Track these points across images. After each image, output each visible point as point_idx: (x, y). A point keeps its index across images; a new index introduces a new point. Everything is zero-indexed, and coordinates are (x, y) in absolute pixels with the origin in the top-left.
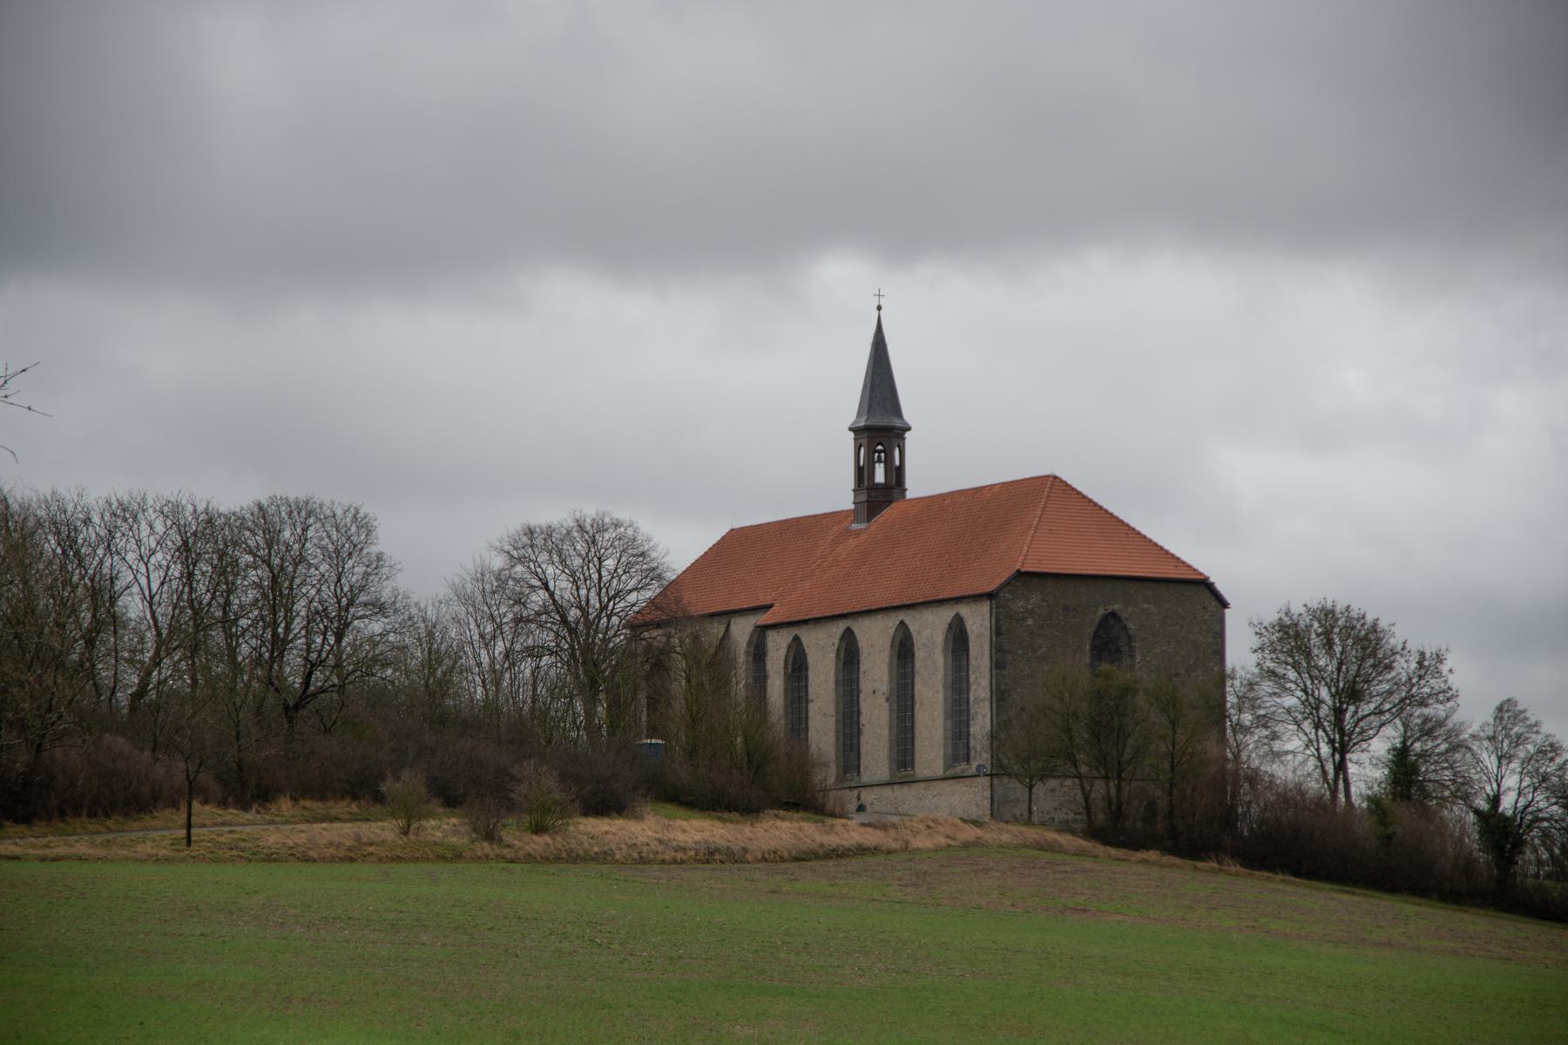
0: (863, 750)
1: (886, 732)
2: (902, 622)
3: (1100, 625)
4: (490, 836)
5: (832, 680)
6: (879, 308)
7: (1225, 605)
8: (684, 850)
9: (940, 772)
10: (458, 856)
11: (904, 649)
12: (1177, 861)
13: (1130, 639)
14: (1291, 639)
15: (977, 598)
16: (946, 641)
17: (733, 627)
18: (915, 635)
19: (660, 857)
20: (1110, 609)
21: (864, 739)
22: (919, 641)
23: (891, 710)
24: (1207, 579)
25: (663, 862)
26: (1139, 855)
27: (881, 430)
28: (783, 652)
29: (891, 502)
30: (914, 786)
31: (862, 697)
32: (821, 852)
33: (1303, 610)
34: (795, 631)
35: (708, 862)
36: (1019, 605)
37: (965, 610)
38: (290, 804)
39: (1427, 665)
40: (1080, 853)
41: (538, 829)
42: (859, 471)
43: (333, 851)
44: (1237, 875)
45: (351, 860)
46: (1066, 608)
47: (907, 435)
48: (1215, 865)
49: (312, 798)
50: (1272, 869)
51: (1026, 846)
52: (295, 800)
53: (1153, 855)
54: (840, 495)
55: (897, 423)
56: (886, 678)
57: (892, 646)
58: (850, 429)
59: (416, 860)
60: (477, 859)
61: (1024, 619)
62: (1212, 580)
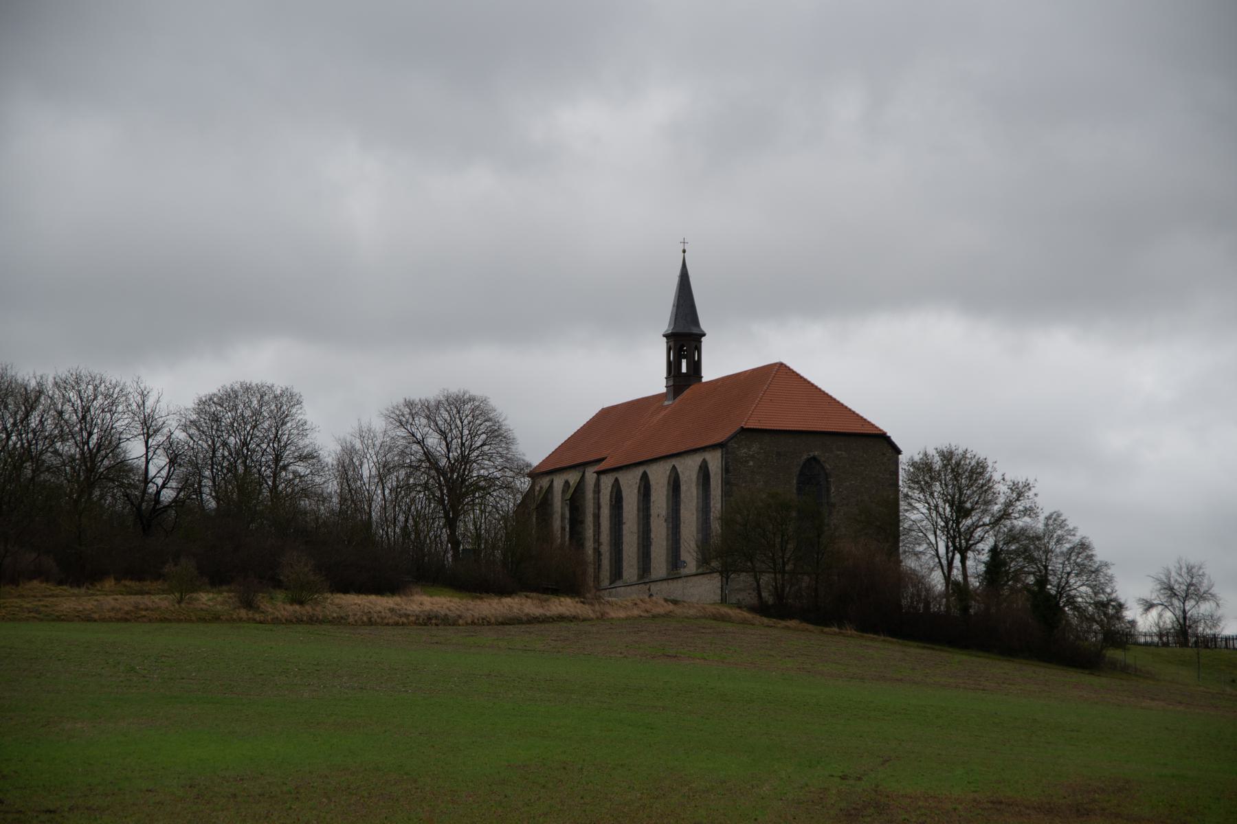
0: (653, 556)
4: (249, 604)
5: (635, 508)
7: (899, 452)
8: (407, 616)
9: (694, 571)
10: (216, 618)
11: (675, 485)
12: (810, 627)
14: (924, 471)
15: (713, 447)
16: (698, 478)
20: (812, 454)
21: (653, 548)
25: (387, 624)
26: (783, 623)
27: (685, 341)
32: (525, 618)
33: (934, 452)
35: (425, 624)
38: (113, 582)
39: (1019, 491)
40: (744, 622)
41: (293, 601)
42: (669, 363)
43: (112, 614)
44: (851, 636)
45: (126, 620)
47: (703, 339)
48: (836, 629)
49: (131, 579)
50: (876, 632)
52: (118, 580)
55: (695, 331)
59: (179, 621)
60: (231, 620)
61: (747, 462)
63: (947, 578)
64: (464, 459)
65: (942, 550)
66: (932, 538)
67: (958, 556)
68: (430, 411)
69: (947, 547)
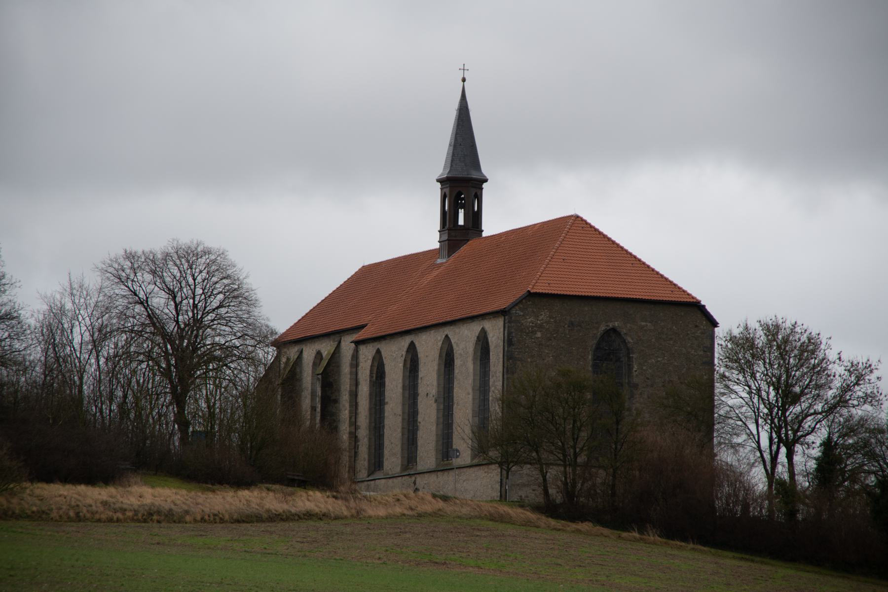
1: (434, 428)
2: (447, 336)
3: (602, 337)
5: (400, 386)
6: (464, 80)
7: (715, 324)
8: (123, 511)
11: (448, 359)
12: (606, 531)
13: (629, 351)
14: (744, 348)
17: (343, 344)
18: (455, 346)
19: (97, 516)
21: (420, 433)
22: (457, 351)
23: (438, 410)
24: (699, 302)
25: (99, 521)
26: (573, 526)
27: (462, 188)
28: (369, 362)
29: (468, 240)
30: (452, 473)
31: (420, 399)
32: (265, 515)
33: (757, 325)
34: (377, 345)
35: (145, 521)
36: (529, 320)
37: (488, 325)
39: (859, 373)
40: (527, 523)
44: (654, 543)
46: (572, 324)
47: (485, 185)
48: (637, 535)
50: (684, 539)
51: (480, 517)
53: (585, 526)
54: (425, 235)
55: (475, 175)
56: (435, 383)
57: (440, 356)
58: (438, 181)
61: (534, 332)
62: (703, 303)
63: (771, 475)
64: (197, 323)
65: (765, 442)
66: (753, 427)
67: (783, 450)
68: (156, 266)
69: (771, 439)
